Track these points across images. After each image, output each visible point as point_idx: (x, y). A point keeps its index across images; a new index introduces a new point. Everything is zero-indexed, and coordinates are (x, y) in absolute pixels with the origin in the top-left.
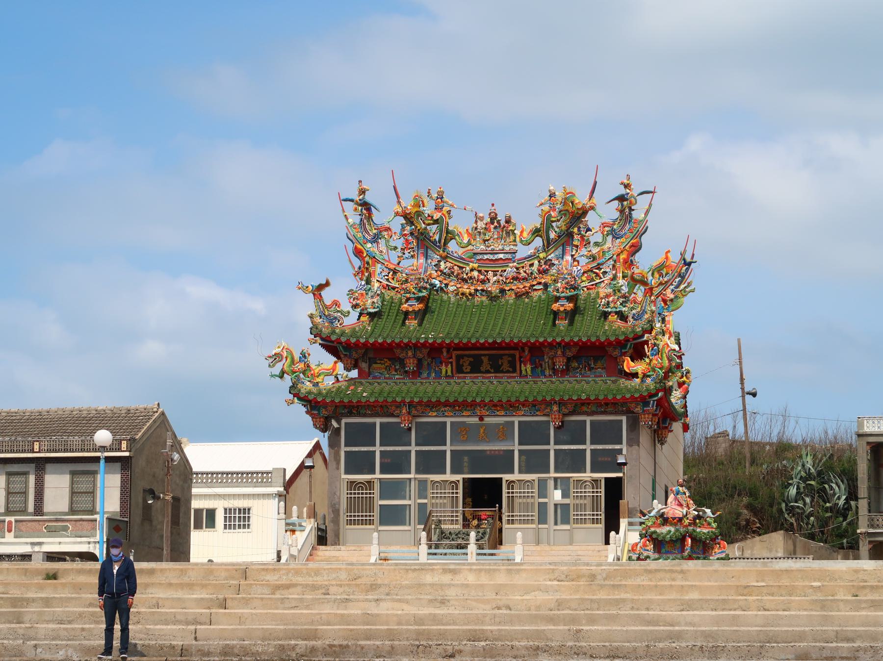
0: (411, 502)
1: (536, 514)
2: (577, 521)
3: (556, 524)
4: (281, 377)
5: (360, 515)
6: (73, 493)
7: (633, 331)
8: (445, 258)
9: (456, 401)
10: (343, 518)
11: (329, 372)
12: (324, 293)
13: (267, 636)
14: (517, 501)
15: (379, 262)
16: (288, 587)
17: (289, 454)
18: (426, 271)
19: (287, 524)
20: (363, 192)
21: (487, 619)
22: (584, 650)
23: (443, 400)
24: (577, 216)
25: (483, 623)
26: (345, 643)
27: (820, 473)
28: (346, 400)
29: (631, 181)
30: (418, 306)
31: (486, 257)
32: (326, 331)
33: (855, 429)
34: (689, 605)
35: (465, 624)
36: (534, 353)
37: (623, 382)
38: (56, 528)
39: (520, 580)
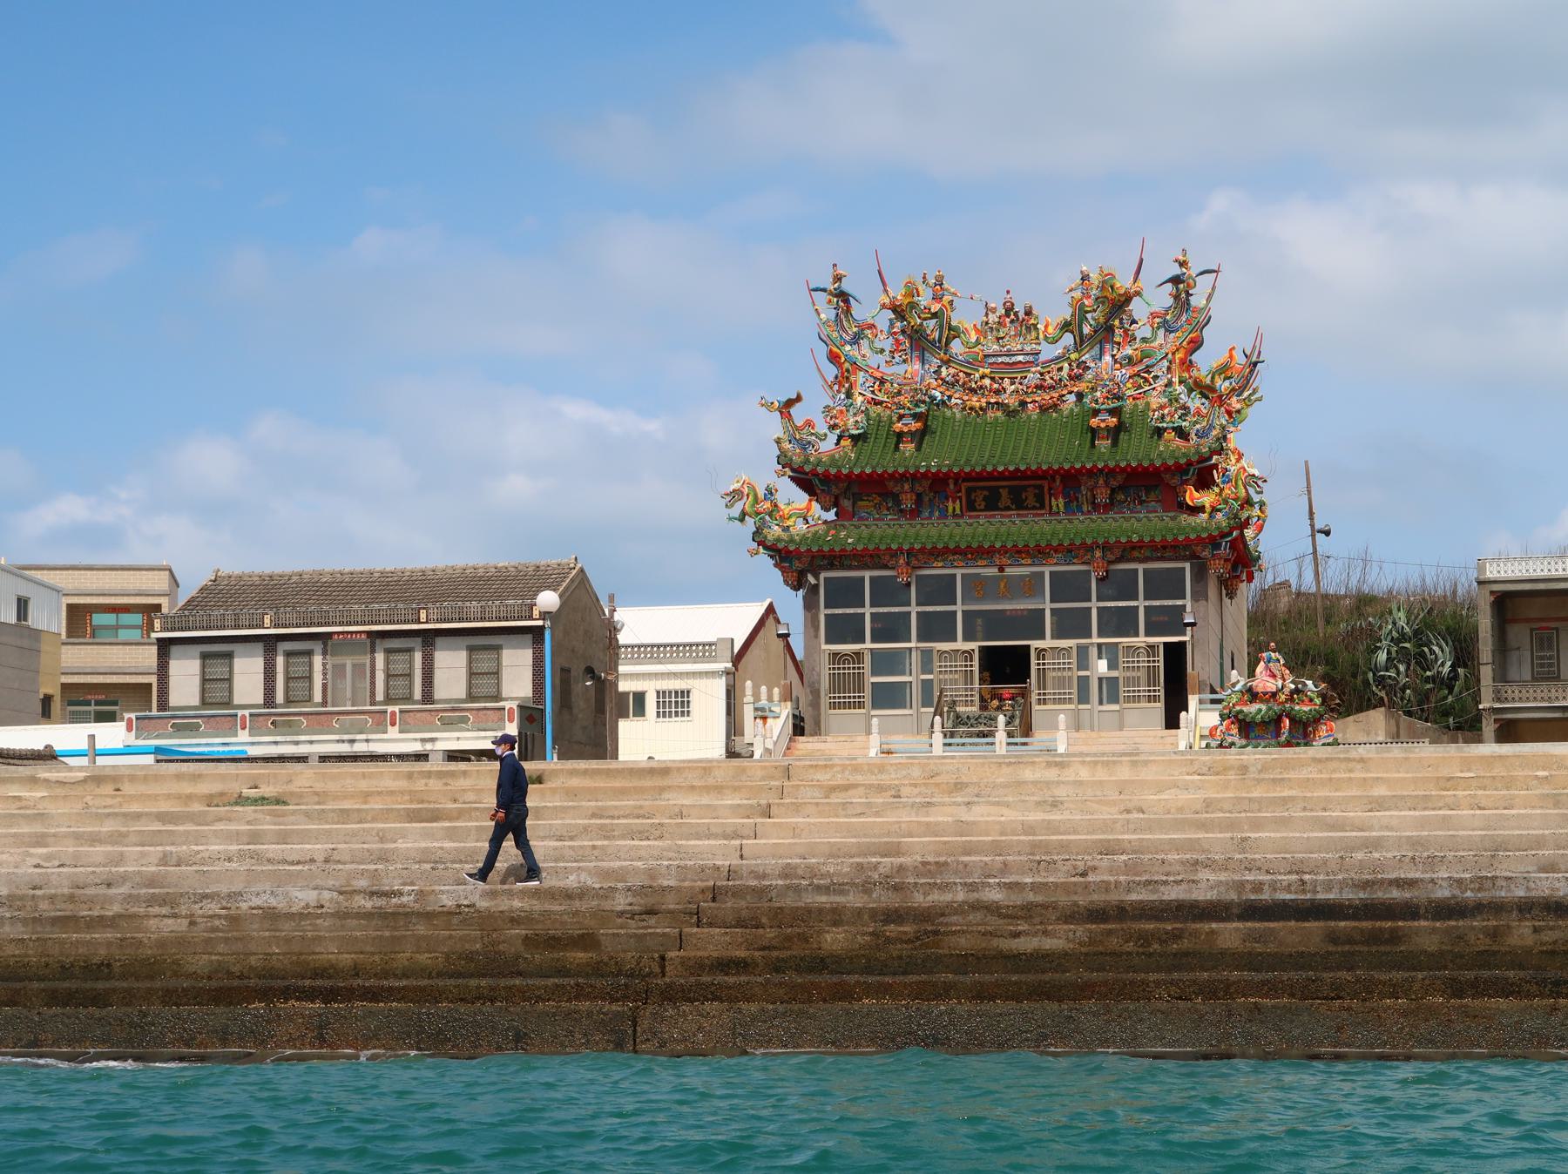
0: (912, 677)
1: (1075, 690)
2: (1128, 700)
3: (1101, 703)
4: (742, 519)
5: (841, 697)
6: (471, 674)
7: (1197, 452)
8: (947, 363)
9: (969, 547)
10: (825, 701)
11: (802, 513)
12: (794, 410)
13: (835, 853)
14: (1050, 675)
15: (861, 369)
16: (846, 788)
17: (736, 621)
18: (922, 379)
19: (756, 709)
20: (838, 278)
21: (1118, 825)
22: (1258, 864)
23: (952, 546)
24: (1118, 304)
25: (1112, 831)
26: (942, 859)
27: (1416, 633)
28: (826, 549)
29: (1189, 258)
30: (915, 426)
31: (1000, 360)
32: (797, 460)
33: (1474, 575)
34: (1379, 804)
35: (1088, 833)
36: (1069, 483)
37: (1185, 519)
38: (453, 718)
39: (1148, 774)
